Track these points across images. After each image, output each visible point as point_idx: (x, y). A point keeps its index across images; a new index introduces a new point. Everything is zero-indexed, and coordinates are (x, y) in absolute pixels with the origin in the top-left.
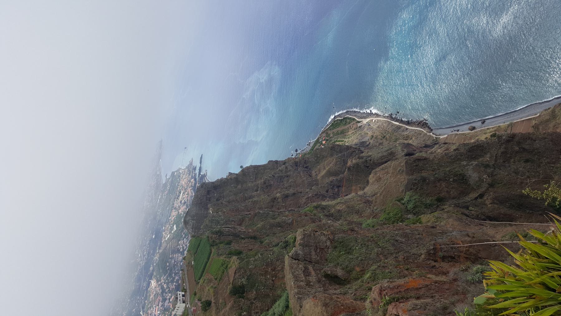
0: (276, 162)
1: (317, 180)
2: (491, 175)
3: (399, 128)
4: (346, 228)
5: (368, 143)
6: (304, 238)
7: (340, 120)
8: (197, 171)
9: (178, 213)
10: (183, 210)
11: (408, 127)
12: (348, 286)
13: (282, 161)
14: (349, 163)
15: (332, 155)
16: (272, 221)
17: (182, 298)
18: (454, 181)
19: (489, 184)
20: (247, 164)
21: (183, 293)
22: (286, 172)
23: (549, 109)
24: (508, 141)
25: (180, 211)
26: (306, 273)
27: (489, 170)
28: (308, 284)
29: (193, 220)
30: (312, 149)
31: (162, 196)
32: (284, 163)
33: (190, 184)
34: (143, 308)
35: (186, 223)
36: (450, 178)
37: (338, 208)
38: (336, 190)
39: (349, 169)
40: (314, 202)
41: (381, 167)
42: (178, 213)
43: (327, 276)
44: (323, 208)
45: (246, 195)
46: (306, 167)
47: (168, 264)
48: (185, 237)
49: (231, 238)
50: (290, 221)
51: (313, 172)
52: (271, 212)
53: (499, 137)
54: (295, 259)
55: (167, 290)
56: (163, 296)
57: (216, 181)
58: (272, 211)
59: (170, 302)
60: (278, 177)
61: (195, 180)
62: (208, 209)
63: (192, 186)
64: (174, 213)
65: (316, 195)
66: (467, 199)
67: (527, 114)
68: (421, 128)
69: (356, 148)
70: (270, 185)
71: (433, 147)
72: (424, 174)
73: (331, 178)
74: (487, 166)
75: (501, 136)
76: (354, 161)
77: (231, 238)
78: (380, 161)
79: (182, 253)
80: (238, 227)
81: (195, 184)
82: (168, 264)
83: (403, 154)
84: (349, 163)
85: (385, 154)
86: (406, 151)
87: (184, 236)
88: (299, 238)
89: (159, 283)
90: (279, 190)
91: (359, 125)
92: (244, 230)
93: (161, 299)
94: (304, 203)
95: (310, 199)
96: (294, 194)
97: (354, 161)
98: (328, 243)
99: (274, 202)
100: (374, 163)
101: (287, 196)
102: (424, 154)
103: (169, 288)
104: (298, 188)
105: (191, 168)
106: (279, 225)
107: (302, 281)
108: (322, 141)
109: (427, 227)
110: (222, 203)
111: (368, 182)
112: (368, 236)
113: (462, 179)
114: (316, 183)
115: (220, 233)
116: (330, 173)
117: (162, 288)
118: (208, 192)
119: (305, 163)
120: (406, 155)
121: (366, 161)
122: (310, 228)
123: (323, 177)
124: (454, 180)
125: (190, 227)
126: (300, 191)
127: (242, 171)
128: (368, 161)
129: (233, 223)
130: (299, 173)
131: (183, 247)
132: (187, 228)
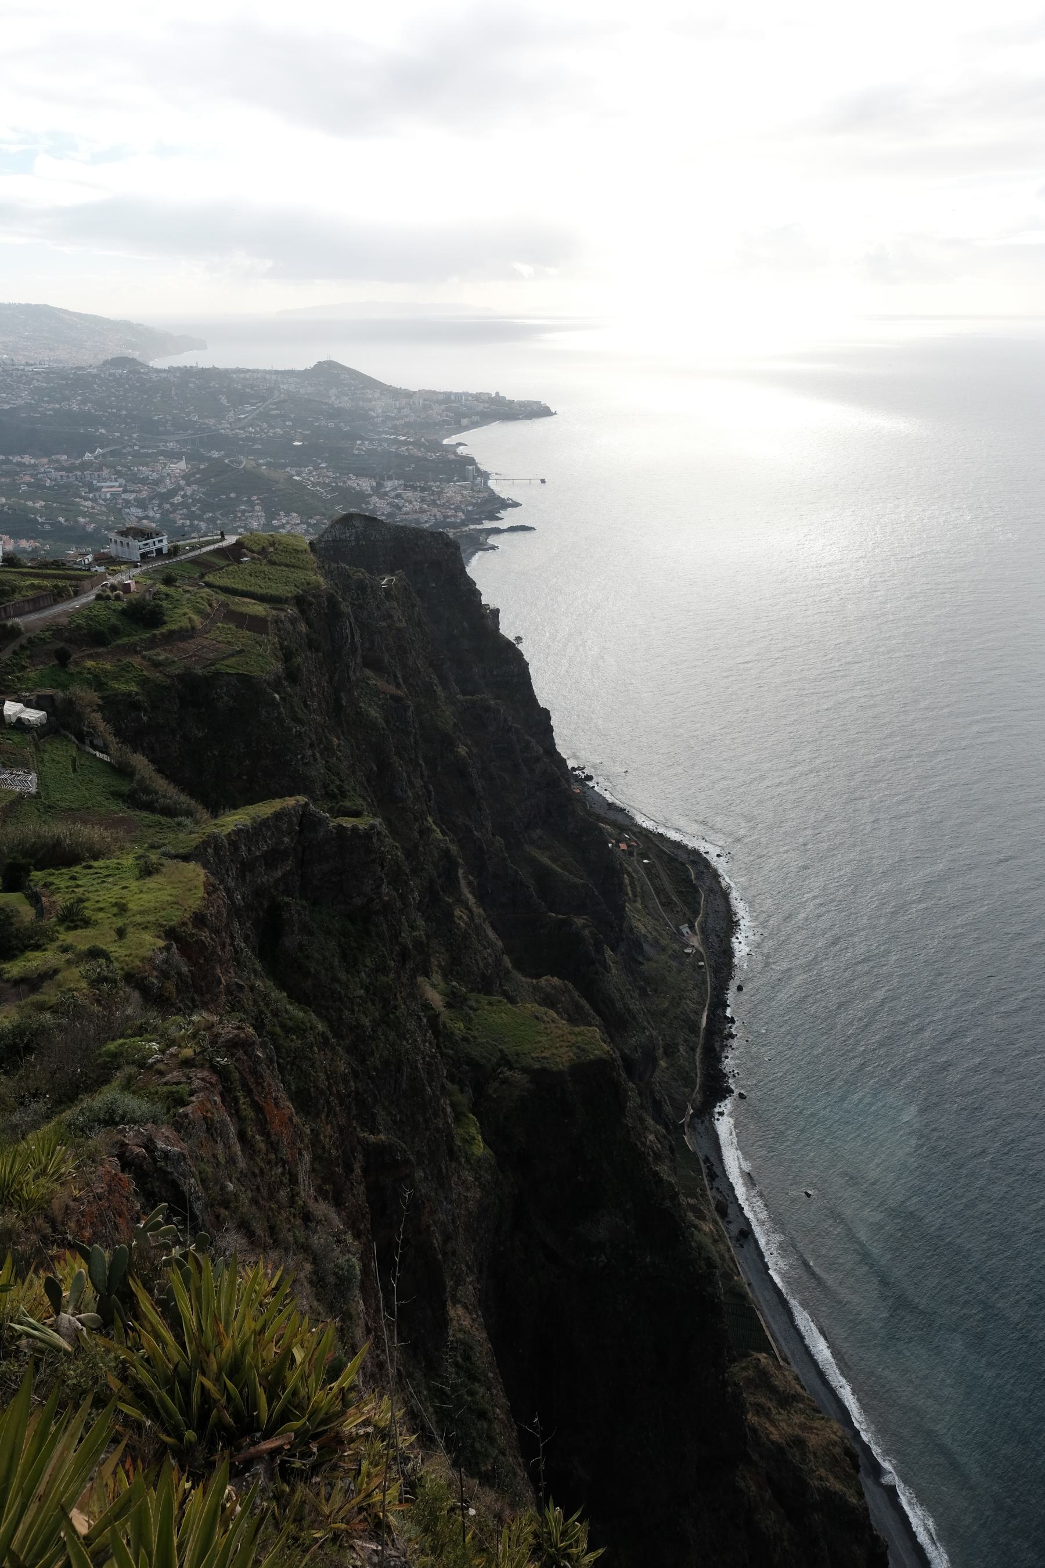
3: (694, 1028)
4: (406, 937)
5: (640, 959)
7: (689, 876)
8: (488, 525)
9: (370, 496)
10: (380, 507)
11: (699, 1050)
12: (258, 967)
17: (153, 548)
20: (526, 649)
21: (165, 551)
23: (802, 1387)
25: (375, 499)
26: (273, 858)
28: (246, 868)
29: (357, 539)
30: (599, 818)
31: (405, 443)
34: (112, 453)
35: (347, 520)
41: (583, 1002)
42: (370, 496)
44: (449, 875)
47: (233, 495)
48: (309, 525)
54: (300, 824)
55: (167, 506)
56: (151, 499)
59: (140, 519)
61: (464, 523)
62: (392, 572)
63: (445, 517)
64: (365, 484)
68: (702, 1085)
69: (621, 930)
71: (657, 1122)
76: (587, 932)
79: (268, 526)
80: (359, 660)
81: (454, 526)
82: (233, 495)
84: (579, 921)
85: (619, 1005)
86: (637, 1055)
87: (313, 521)
89: (182, 483)
91: (685, 929)
92: (353, 678)
93: (144, 495)
98: (358, 901)
102: (633, 1101)
103: (174, 511)
107: (250, 850)
108: (625, 840)
109: (450, 1137)
110: (414, 606)
112: (396, 998)
115: (334, 612)
117: (173, 493)
120: (625, 1058)
122: (391, 848)
129: (367, 645)
131: (283, 526)
132: (332, 526)
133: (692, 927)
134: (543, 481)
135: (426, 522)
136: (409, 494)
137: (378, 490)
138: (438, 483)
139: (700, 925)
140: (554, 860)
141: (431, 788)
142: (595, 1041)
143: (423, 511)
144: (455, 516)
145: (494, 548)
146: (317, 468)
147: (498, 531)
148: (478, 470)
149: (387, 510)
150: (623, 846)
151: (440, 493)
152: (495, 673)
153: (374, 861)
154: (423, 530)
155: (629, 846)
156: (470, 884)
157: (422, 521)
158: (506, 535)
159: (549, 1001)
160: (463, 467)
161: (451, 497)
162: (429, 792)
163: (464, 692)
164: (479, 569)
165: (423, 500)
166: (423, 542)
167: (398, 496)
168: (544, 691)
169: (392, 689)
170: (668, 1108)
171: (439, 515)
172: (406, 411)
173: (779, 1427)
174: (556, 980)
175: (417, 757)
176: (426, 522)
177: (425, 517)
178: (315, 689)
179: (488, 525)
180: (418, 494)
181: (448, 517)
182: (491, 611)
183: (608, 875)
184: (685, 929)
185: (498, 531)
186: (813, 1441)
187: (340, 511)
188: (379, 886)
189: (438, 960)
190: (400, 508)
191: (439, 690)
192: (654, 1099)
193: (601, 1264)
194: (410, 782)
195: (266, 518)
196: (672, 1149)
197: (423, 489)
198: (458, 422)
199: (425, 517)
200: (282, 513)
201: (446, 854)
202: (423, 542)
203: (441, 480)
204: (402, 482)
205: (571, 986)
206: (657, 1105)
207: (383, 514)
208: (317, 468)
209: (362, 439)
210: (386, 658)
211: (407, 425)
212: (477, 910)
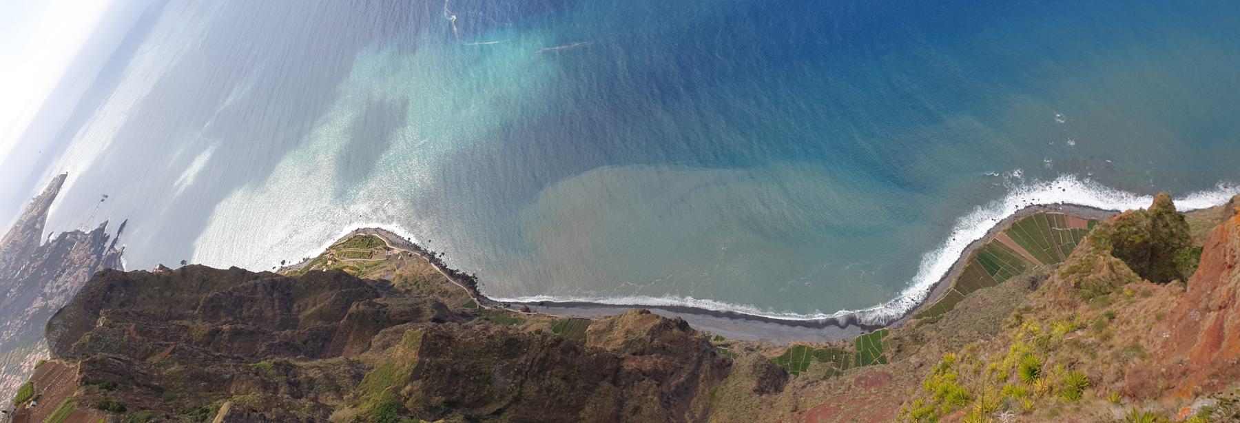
1: (297, 320)
8: (108, 245)
10: (58, 302)
22: (252, 293)
24: (552, 345)
40: (279, 354)
44: (288, 368)
53: (545, 336)
58: (205, 352)
62: (98, 316)
64: (38, 303)
81: (97, 264)
84: (353, 308)
85: (407, 309)
95: (273, 350)
96: (252, 333)
105: (99, 236)
106: (207, 378)
111: (370, 345)
116: (321, 315)
120: (434, 320)
123: (309, 317)
126: (264, 329)
127: (183, 269)
130: (273, 300)
136: (61, 279)
146: (7, 328)
147: (115, 241)
149: (62, 298)
151: (72, 262)
154: (87, 288)
156: (301, 359)
159: (386, 346)
160: (65, 241)
163: (194, 308)
164: (127, 265)
165: (70, 274)
167: (58, 287)
168: (151, 267)
170: (468, 310)
172: (7, 257)
173: (617, 339)
177: (81, 278)
179: (108, 245)
183: (339, 277)
185: (115, 241)
186: (629, 326)
187: (43, 327)
189: (329, 399)
190: (66, 290)
191: (185, 323)
196: (487, 319)
197: (64, 271)
198: (36, 230)
199: (81, 278)
201: (277, 365)
206: (464, 315)
208: (7, 328)
209: (8, 291)
211: (17, 260)
212: (314, 363)
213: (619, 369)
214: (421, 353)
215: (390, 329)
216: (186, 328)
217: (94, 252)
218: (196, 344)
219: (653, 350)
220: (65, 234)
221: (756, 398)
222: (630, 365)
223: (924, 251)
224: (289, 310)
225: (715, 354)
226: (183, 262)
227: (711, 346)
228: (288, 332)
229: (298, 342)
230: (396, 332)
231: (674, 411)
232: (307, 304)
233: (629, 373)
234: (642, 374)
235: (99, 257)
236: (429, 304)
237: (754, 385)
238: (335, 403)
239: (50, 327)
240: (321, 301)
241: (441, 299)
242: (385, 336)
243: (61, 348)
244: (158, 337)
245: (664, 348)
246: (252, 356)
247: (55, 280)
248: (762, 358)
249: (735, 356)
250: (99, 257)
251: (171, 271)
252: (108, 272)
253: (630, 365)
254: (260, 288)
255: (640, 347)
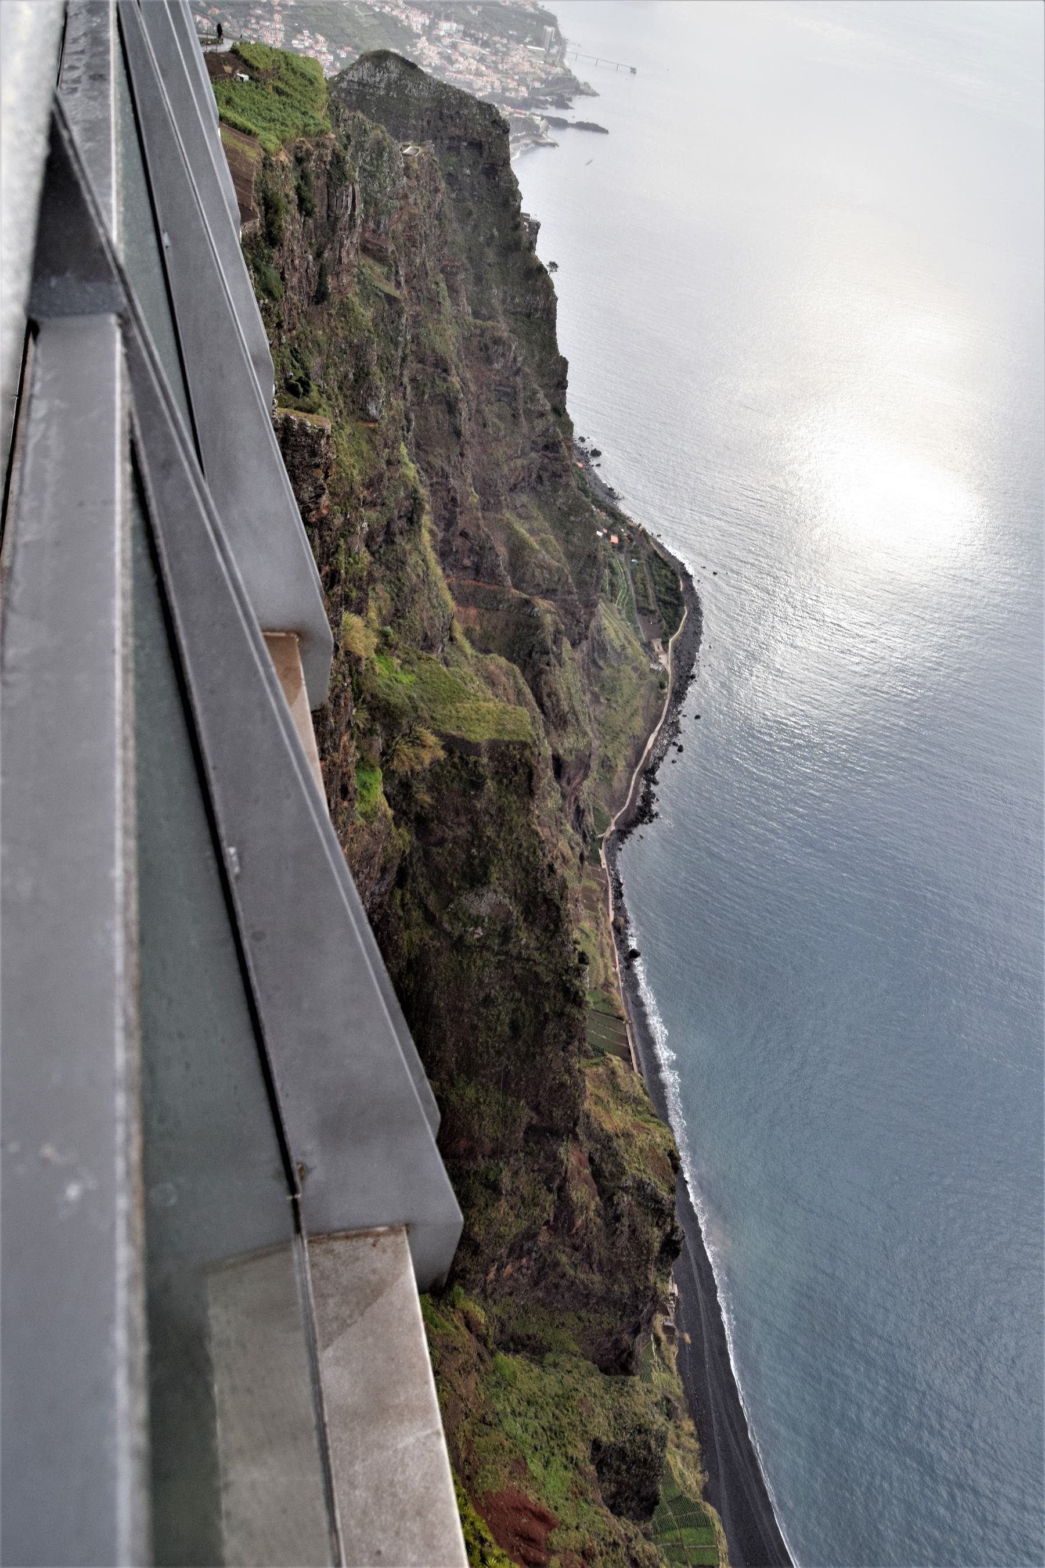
0: (562, 385)
1: (498, 506)
2: (483, 946)
5: (601, 663)
6: (307, 435)
8: (553, 112)
10: (428, 56)
13: (563, 402)
14: (542, 605)
15: (571, 556)
16: (374, 353)
18: (471, 857)
19: (461, 937)
22: (528, 413)
24: (566, 991)
25: (423, 42)
27: (495, 943)
29: (388, 87)
32: (559, 411)
33: (512, 85)
36: (479, 847)
37: (413, 559)
38: (467, 562)
39: (527, 602)
40: (434, 493)
41: (527, 690)
42: (419, 36)
43: (639, 1326)
44: (412, 518)
45: (462, 276)
46: (540, 477)
49: (320, 211)
50: (373, 411)
51: (524, 498)
52: (400, 353)
53: (578, 972)
57: (510, 174)
58: (404, 359)
60: (514, 388)
62: (420, 142)
63: (505, 89)
64: (418, 21)
65: (454, 500)
66: (423, 885)
67: (640, 1054)
69: (587, 627)
70: (489, 361)
72: (490, 785)
73: (502, 551)
74: (506, 935)
75: (579, 975)
77: (320, 211)
78: (545, 691)
83: (561, 752)
84: (542, 605)
86: (569, 759)
88: (311, 422)
90: (473, 388)
91: (657, 644)
92: (345, 260)
94: (429, 463)
95: (439, 481)
96: (458, 434)
97: (548, 619)
99: (436, 366)
100: (541, 672)
101: (451, 407)
104: (478, 449)
105: (565, 89)
106: (362, 375)
110: (437, 190)
111: (487, 651)
113: (476, 878)
114: (490, 502)
116: (518, 549)
118: (477, 146)
119: (555, 475)
121: (548, 653)
123: (509, 526)
124: (474, 858)
125: (364, 72)
126: (468, 452)
127: (541, 269)
128: (545, 658)
129: (371, 225)
130: (524, 454)
133: (665, 643)
134: (633, 71)
135: (480, 90)
136: (467, 46)
137: (429, 31)
138: (505, 41)
139: (674, 643)
140: (531, 531)
141: (412, 416)
142: (524, 720)
143: (479, 74)
144: (517, 91)
145: (553, 145)
147: (560, 124)
148: (557, 34)
149: (436, 61)
150: (614, 539)
152: (517, 300)
153: (317, 466)
154: (464, 99)
155: (620, 540)
157: (476, 86)
158: (570, 132)
159: (491, 681)
161: (517, 64)
162: (409, 421)
165: (482, 59)
166: (466, 112)
169: (390, 288)
170: (590, 819)
171: (497, 84)
174: (503, 661)
175: (402, 374)
176: (480, 90)
178: (297, 262)
179: (553, 112)
180: (477, 49)
181: (509, 90)
182: (530, 224)
184: (657, 644)
187: (376, 46)
188: (319, 496)
191: (447, 303)
192: (578, 807)
193: (476, 936)
194: (388, 401)
195: (286, 35)
197: (485, 44)
199: (479, 83)
200: (306, 32)
201: (413, 496)
202: (466, 112)
203: (510, 38)
204: (462, 27)
205: (517, 670)
206: (579, 813)
207: (430, 65)
210: (391, 248)
213: (556, 1134)
214: (494, 745)
215: (521, 681)
216: (434, 302)
217: (533, 91)
218: (415, 339)
219: (607, 1196)
220: (551, 20)
221: (581, 1451)
222: (571, 1156)
223: (663, 1093)
224: (513, 489)
225: (636, 1331)
226: (554, 265)
227: (649, 1321)
228: (475, 499)
229: (461, 522)
230: (519, 693)
231: (509, 1269)
232: (528, 518)
233: (553, 1157)
234: (555, 1180)
235: (526, 104)
236: (582, 744)
237: (607, 1439)
238: (373, 614)
239: (380, 58)
240: (543, 543)
241: (594, 764)
242: (507, 674)
243: (351, 95)
244: (410, 263)
245: (617, 1218)
246: (418, 446)
247: (465, 34)
248: (662, 1440)
249: (647, 1378)
250: (526, 104)
251: (532, 246)
252: (501, 127)
253: (571, 1156)
254: (540, 425)
255: (608, 1168)
